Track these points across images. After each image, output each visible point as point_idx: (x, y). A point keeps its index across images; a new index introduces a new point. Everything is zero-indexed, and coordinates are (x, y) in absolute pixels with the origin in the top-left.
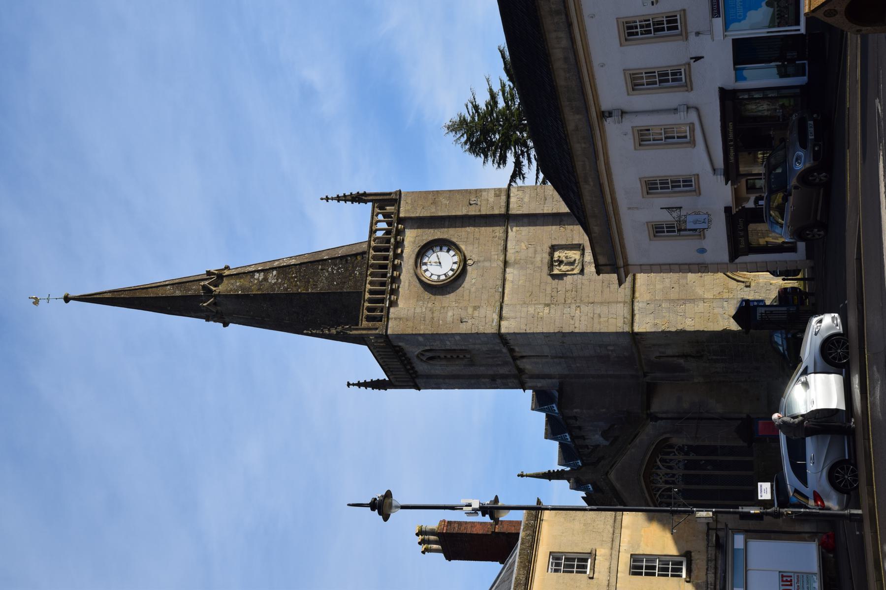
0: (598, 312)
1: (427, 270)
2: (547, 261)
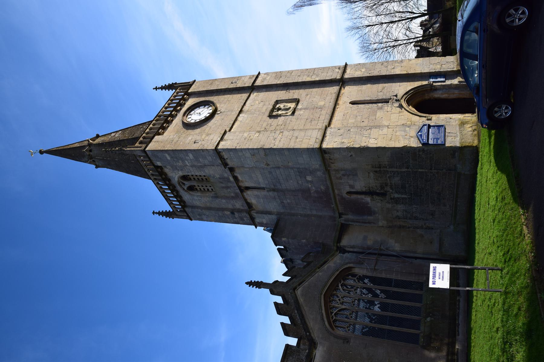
0: (296, 135)
2: (270, 109)
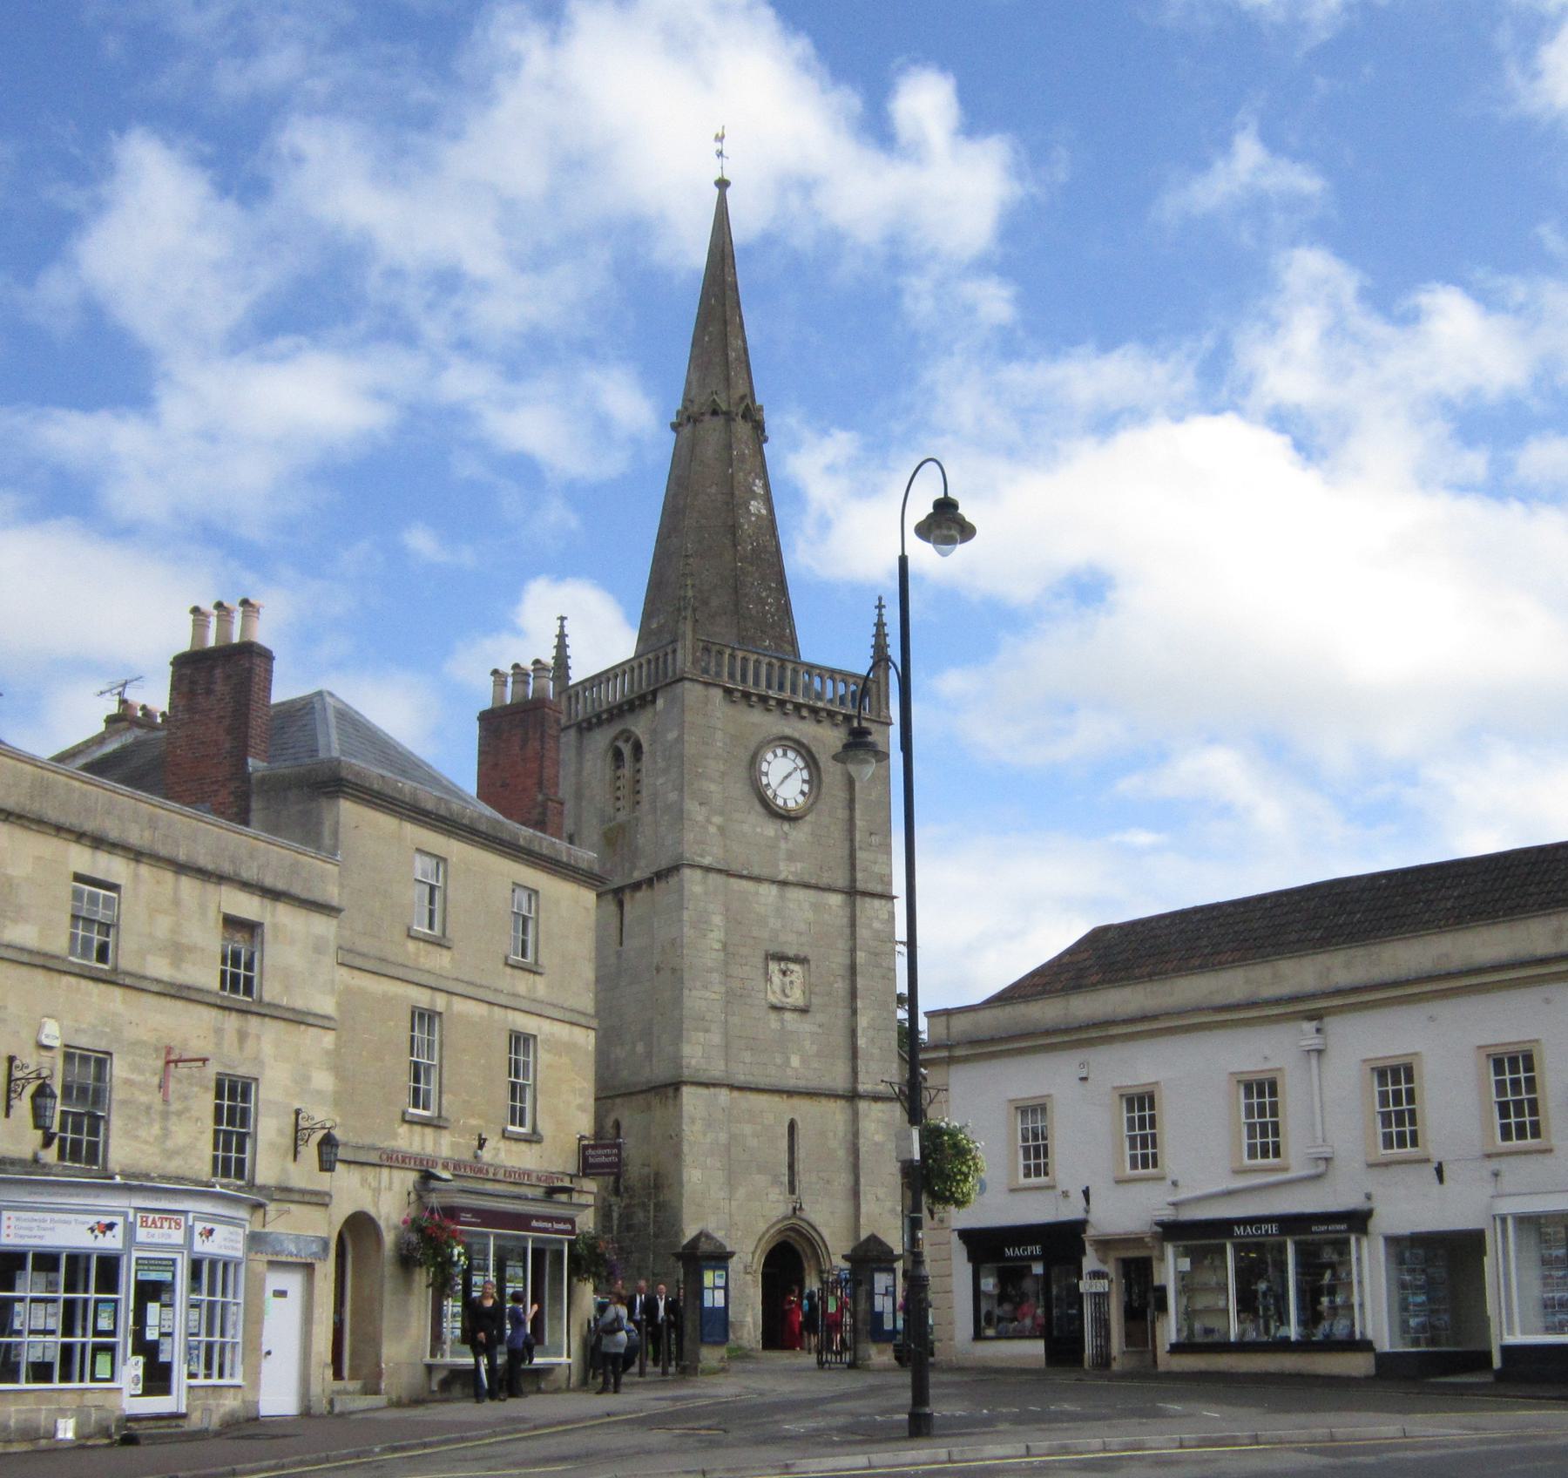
1: (776, 756)
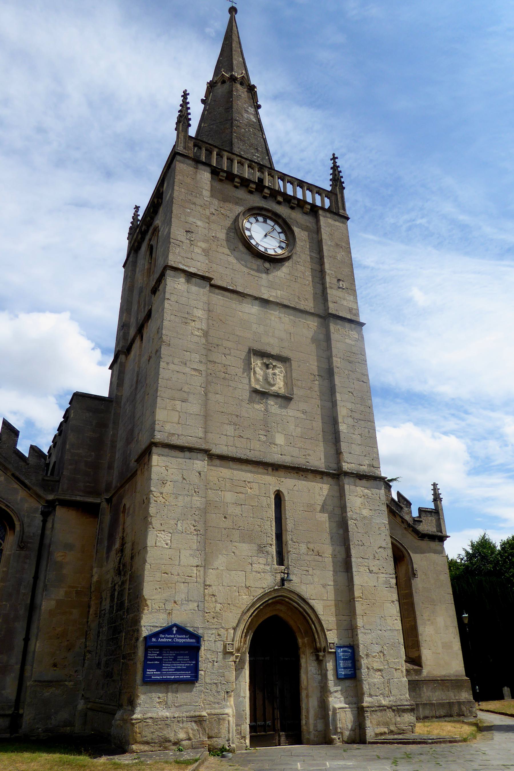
0: (190, 399)
